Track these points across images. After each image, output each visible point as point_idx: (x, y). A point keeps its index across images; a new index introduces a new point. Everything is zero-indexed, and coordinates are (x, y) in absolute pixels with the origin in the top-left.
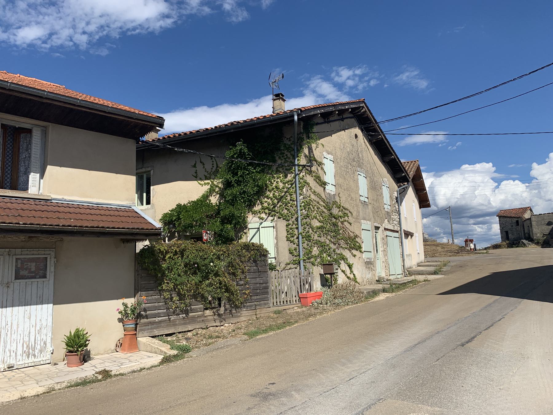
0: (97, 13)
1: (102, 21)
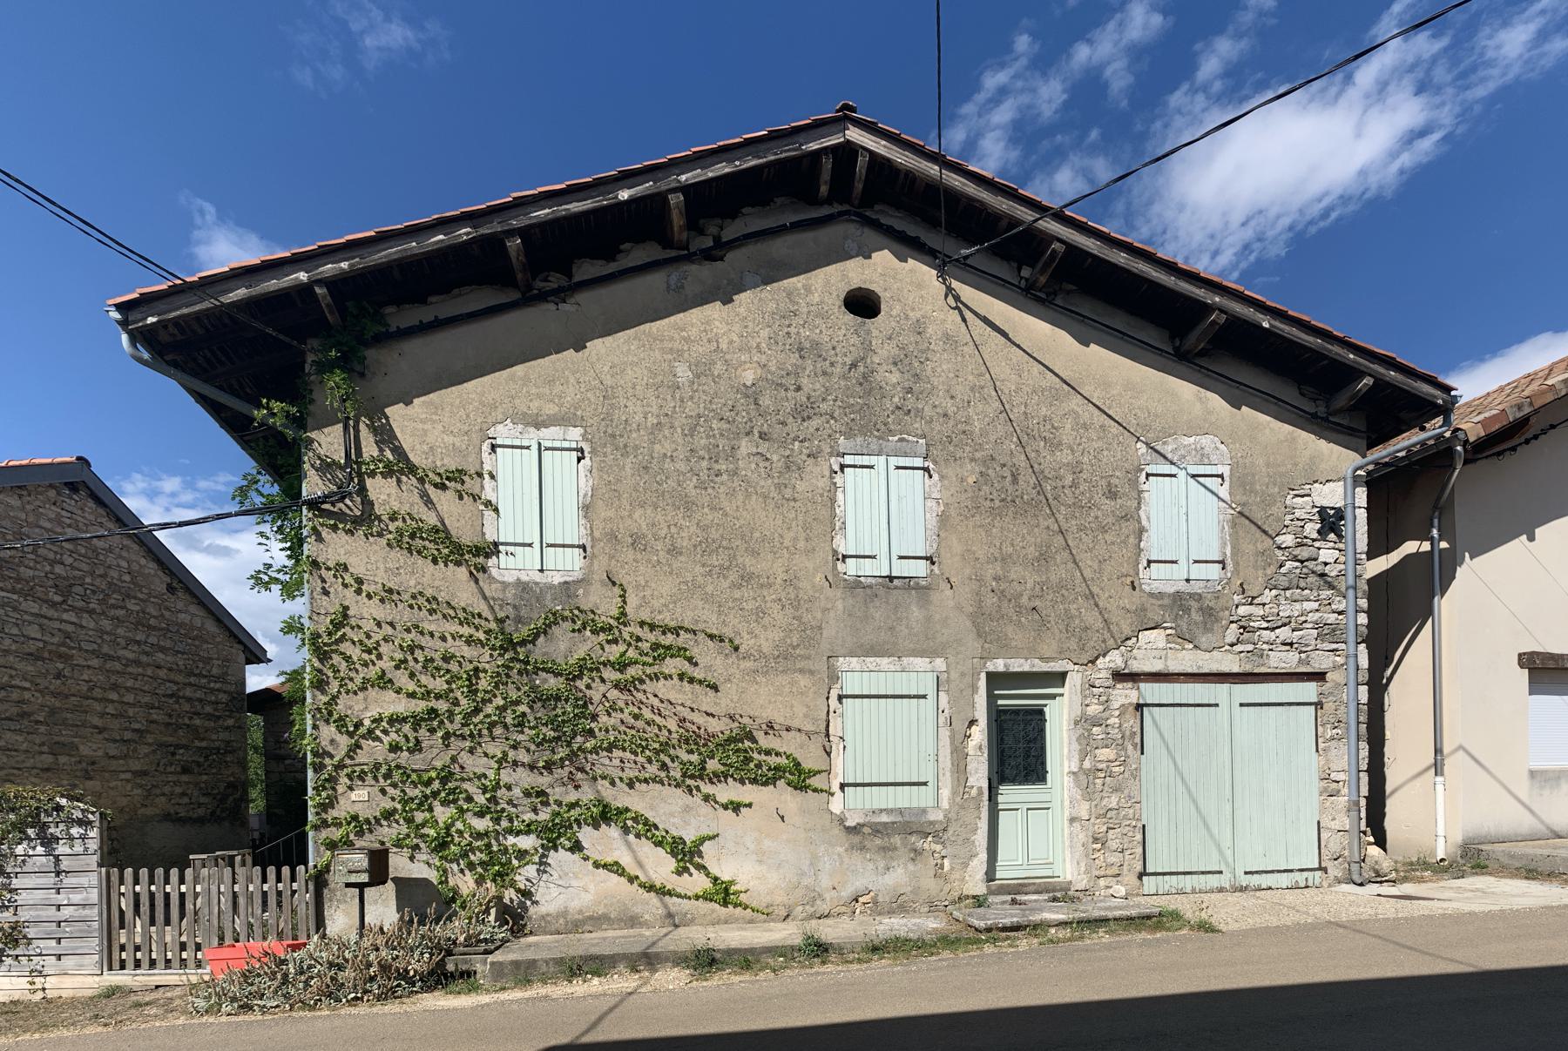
0: (1237, 218)
1: (1248, 233)
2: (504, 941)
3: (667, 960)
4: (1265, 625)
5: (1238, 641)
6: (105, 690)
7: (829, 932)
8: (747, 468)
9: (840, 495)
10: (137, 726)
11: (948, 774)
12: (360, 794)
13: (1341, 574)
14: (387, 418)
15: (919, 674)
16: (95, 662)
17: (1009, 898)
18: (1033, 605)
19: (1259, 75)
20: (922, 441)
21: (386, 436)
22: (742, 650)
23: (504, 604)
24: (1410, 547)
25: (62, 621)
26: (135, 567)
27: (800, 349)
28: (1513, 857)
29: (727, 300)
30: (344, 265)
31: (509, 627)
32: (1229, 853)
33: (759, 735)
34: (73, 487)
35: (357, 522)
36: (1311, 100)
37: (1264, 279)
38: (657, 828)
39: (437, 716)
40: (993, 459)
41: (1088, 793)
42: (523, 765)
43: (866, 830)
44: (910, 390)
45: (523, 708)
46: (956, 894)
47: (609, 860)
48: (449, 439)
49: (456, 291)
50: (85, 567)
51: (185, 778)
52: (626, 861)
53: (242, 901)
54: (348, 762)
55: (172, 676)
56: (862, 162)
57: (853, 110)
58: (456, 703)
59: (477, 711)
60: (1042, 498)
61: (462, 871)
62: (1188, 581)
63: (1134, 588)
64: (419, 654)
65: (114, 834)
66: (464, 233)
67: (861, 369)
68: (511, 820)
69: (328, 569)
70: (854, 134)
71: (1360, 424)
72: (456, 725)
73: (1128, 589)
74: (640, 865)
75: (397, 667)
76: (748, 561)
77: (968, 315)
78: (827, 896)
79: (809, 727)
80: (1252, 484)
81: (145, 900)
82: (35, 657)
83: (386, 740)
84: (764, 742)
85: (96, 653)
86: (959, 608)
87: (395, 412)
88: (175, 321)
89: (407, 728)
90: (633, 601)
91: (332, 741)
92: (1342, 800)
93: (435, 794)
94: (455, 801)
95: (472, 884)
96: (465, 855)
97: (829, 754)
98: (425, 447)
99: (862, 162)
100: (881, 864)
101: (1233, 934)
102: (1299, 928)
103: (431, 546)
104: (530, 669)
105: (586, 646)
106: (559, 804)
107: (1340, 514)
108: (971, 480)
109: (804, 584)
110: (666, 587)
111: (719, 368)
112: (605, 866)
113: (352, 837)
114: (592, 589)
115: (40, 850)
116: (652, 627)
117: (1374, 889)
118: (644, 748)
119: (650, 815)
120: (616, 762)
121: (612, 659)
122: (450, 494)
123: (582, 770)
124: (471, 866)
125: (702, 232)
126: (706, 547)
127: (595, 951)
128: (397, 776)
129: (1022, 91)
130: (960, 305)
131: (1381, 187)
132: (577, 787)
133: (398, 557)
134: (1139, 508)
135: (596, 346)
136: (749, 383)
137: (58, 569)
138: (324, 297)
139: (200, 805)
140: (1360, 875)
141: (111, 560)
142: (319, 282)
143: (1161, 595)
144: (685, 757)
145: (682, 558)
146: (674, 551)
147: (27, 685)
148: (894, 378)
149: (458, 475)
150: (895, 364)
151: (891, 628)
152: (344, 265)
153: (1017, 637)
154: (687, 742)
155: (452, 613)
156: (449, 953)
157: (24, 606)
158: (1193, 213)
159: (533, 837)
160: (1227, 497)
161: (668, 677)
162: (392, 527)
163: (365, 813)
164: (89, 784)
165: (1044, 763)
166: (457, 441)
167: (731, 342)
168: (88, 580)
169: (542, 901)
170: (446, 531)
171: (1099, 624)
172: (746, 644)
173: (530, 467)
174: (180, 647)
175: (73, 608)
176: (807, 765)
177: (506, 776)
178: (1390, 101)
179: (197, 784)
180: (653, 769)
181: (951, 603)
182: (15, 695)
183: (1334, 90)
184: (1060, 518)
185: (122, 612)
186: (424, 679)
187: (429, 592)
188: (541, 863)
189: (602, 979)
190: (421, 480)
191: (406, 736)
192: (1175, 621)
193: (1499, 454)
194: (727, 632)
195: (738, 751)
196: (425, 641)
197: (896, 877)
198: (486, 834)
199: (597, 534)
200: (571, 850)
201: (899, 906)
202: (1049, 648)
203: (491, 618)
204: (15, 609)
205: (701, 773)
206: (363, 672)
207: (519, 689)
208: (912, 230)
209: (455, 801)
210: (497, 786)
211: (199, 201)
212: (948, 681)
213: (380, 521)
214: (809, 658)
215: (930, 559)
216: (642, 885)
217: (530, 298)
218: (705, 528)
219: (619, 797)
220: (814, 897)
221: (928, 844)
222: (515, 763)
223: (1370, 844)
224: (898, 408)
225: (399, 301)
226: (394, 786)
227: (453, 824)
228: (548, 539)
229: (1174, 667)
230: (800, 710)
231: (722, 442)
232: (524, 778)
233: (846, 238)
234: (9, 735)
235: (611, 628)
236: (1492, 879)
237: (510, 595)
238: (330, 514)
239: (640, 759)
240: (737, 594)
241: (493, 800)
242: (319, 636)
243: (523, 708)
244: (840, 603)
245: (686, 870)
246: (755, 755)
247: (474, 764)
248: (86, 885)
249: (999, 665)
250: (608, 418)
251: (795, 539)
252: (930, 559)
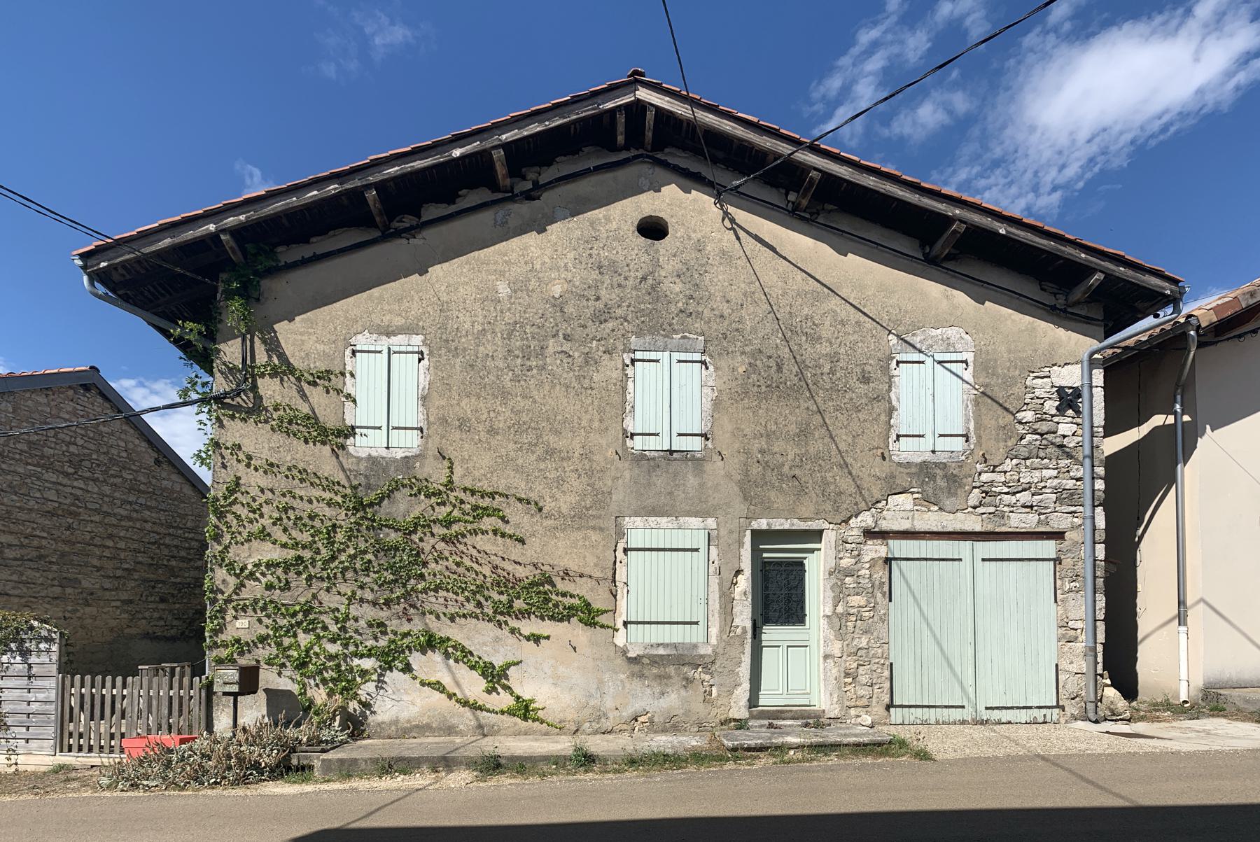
0: (1083, 135)
1: (1094, 148)
2: (342, 743)
3: (461, 763)
4: (1006, 490)
5: (981, 504)
6: (103, 539)
7: (597, 745)
8: (553, 364)
9: (630, 384)
10: (126, 566)
11: (717, 615)
12: (243, 623)
13: (1079, 445)
14: (275, 332)
15: (693, 531)
16: (97, 518)
17: (766, 722)
18: (792, 473)
19: (1106, 15)
20: (701, 338)
21: (273, 346)
22: (544, 511)
23: (358, 474)
24: (1158, 420)
25: (73, 487)
26: (131, 446)
27: (600, 267)
28: (1247, 702)
29: (541, 230)
30: (242, 217)
31: (361, 492)
32: (971, 691)
33: (557, 580)
34: (86, 388)
35: (250, 412)
36: (1153, 32)
37: (1108, 187)
38: (472, 654)
39: (303, 562)
40: (760, 352)
41: (840, 634)
42: (368, 602)
43: (646, 661)
44: (691, 297)
45: (369, 556)
46: (723, 717)
47: (433, 680)
48: (321, 347)
49: (331, 233)
50: (93, 447)
51: (162, 606)
52: (447, 681)
53: (154, 703)
54: (235, 597)
55: (156, 528)
56: (650, 115)
57: (642, 74)
58: (318, 552)
59: (333, 558)
60: (803, 383)
61: (317, 685)
62: (934, 452)
63: (884, 459)
64: (291, 514)
65: (70, 649)
66: (333, 188)
67: (650, 281)
68: (357, 646)
69: (227, 448)
70: (643, 94)
71: (1099, 315)
72: (317, 570)
73: (879, 459)
74: (458, 684)
75: (274, 524)
76: (552, 439)
77: (741, 234)
78: (611, 715)
79: (598, 574)
80: (994, 368)
81: (87, 699)
82: (52, 514)
83: (264, 580)
84: (561, 586)
85: (98, 511)
86: (729, 476)
87: (282, 328)
88: (123, 264)
89: (280, 571)
90: (458, 471)
91: (224, 581)
92: (1080, 646)
93: (299, 624)
94: (314, 630)
95: (324, 696)
96: (320, 673)
97: (615, 596)
98: (303, 354)
99: (650, 115)
100: (658, 690)
101: (944, 762)
102: (1010, 759)
103: (303, 429)
104: (376, 526)
105: (421, 506)
106: (395, 633)
107: (1077, 393)
108: (741, 370)
109: (597, 457)
110: (485, 460)
111: (533, 283)
112: (429, 685)
113: (235, 656)
114: (427, 462)
115: (19, 659)
116: (473, 492)
117: (1108, 726)
118: (463, 590)
119: (466, 644)
120: (441, 600)
121: (440, 517)
122: (320, 388)
123: (414, 606)
124: (324, 681)
125: (524, 178)
126: (519, 428)
127: (406, 754)
128: (270, 608)
129: (892, 43)
130: (734, 226)
131: (1218, 103)
132: (409, 620)
133: (279, 438)
134: (890, 390)
135: (436, 271)
136: (557, 296)
137: (73, 449)
138: (228, 242)
139: (172, 627)
140: (1095, 713)
141: (112, 441)
142: (224, 231)
143: (909, 465)
144: (496, 597)
145: (499, 437)
146: (492, 431)
147: (45, 535)
148: (678, 288)
149: (326, 375)
150: (679, 276)
151: (670, 493)
152: (242, 217)
153: (778, 500)
154: (498, 585)
155: (318, 481)
156: (294, 750)
157: (46, 476)
158: (1043, 134)
159: (373, 659)
160: (971, 380)
161: (484, 532)
162: (275, 416)
163: (246, 637)
164: (88, 609)
165: (803, 608)
166: (327, 349)
167: (544, 263)
168: (94, 456)
169: (379, 712)
170: (316, 418)
171: (853, 489)
172: (548, 505)
173: (382, 368)
174: (162, 506)
175: (82, 478)
176: (596, 605)
177: (354, 611)
178: (1226, 29)
179: (171, 611)
180: (470, 607)
181: (723, 473)
182: (35, 543)
183: (1174, 22)
184: (819, 400)
185: (118, 480)
186: (294, 533)
187: (301, 466)
188: (379, 681)
189: (407, 777)
190: (299, 379)
191: (278, 578)
192: (921, 486)
193: (1239, 336)
194: (533, 496)
195: (539, 592)
196: (296, 503)
197: (672, 701)
198: (337, 656)
199: (432, 419)
200: (403, 670)
201: (672, 725)
202: (807, 509)
203: (347, 485)
204: (39, 479)
205: (509, 610)
206: (249, 527)
207: (366, 541)
208: (695, 167)
209: (314, 630)
210: (347, 618)
211: (250, 167)
212: (718, 537)
213: (267, 411)
214: (599, 517)
215: (704, 436)
216: (458, 701)
217: (388, 235)
218: (518, 413)
219: (443, 629)
220: (600, 716)
221: (699, 674)
222: (362, 600)
223: (1107, 686)
224: (681, 311)
225: (288, 242)
226: (268, 616)
227: (311, 648)
228: (394, 423)
229: (920, 526)
230: (591, 560)
231: (533, 343)
232: (369, 613)
233: (639, 176)
234: (29, 572)
235: (440, 493)
236: (1224, 721)
237: (362, 467)
238: (229, 406)
239: (461, 598)
240: (542, 466)
241: (343, 629)
242: (218, 500)
243: (369, 556)
244: (627, 472)
245: (494, 689)
246: (554, 597)
247: (330, 600)
248: (48, 688)
249: (763, 524)
250: (443, 326)
251: (591, 420)
252: (704, 436)
